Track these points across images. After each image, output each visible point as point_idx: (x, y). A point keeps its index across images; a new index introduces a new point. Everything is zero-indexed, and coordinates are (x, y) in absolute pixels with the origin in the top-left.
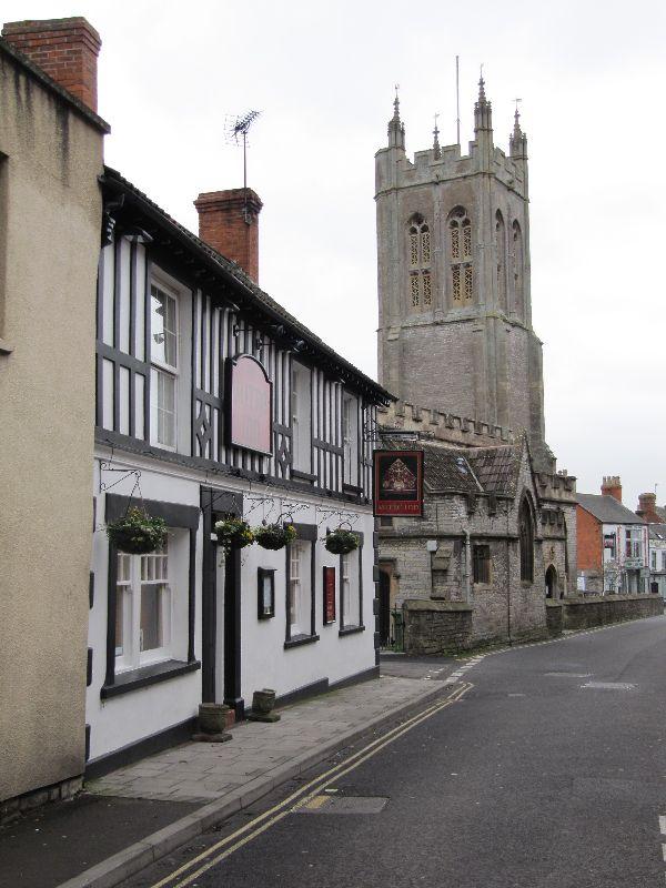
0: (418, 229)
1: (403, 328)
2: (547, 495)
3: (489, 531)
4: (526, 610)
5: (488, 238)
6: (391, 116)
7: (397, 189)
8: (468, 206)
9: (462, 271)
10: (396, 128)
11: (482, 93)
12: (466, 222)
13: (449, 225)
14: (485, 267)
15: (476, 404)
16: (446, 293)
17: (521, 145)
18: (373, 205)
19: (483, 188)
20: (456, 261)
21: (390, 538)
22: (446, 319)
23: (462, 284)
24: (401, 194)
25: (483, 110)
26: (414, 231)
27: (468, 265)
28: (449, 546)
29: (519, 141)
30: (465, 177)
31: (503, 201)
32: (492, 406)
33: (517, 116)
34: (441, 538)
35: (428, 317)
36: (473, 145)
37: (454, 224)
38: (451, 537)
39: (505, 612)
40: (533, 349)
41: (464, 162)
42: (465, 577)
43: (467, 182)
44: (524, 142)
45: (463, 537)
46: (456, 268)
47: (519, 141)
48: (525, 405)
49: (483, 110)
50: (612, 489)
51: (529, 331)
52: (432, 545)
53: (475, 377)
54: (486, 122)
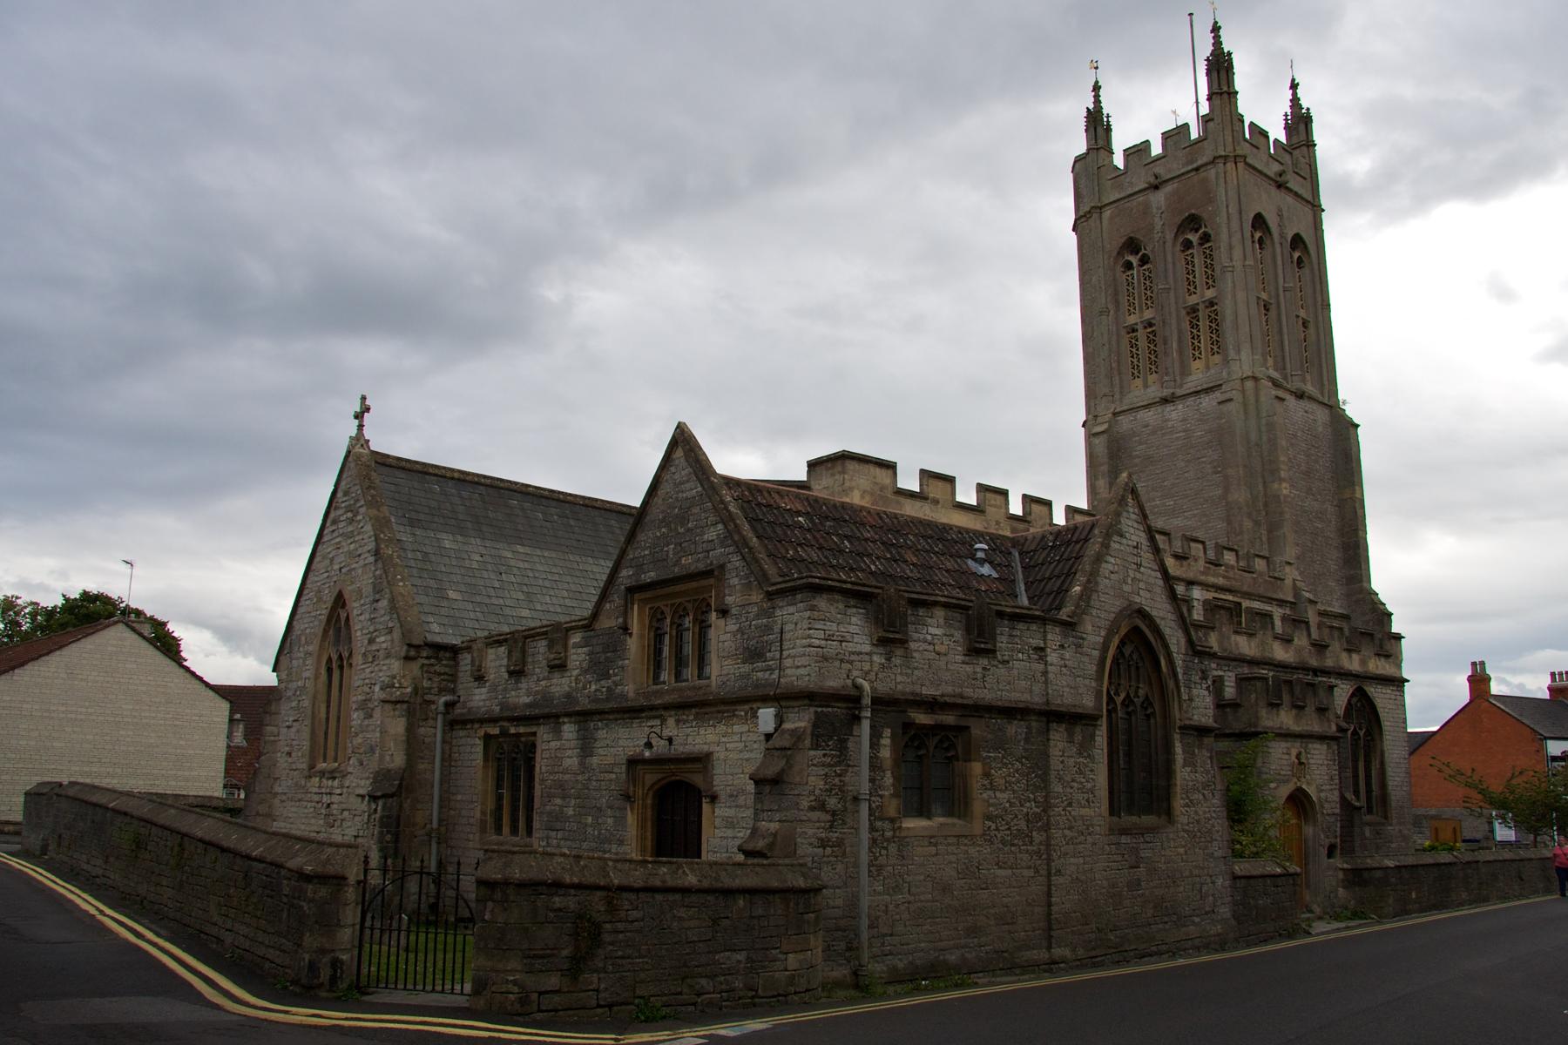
0: (1134, 260)
1: (1114, 414)
2: (1329, 663)
3: (968, 692)
5: (1237, 254)
9: (1202, 313)
10: (1097, 124)
11: (1295, 101)
12: (1206, 238)
13: (1178, 247)
14: (1238, 301)
15: (1229, 523)
16: (1181, 352)
20: (1193, 300)
22: (1179, 392)
24: (1107, 213)
25: (1220, 67)
26: (1129, 266)
27: (1211, 303)
28: (800, 720)
29: (1299, 122)
30: (1197, 169)
31: (1267, 202)
32: (1257, 523)
33: (1294, 86)
34: (784, 699)
35: (1155, 392)
36: (1206, 120)
38: (809, 697)
40: (1344, 431)
42: (856, 799)
43: (1202, 174)
45: (851, 699)
46: (1193, 310)
47: (1299, 122)
52: (766, 716)
54: (1224, 82)
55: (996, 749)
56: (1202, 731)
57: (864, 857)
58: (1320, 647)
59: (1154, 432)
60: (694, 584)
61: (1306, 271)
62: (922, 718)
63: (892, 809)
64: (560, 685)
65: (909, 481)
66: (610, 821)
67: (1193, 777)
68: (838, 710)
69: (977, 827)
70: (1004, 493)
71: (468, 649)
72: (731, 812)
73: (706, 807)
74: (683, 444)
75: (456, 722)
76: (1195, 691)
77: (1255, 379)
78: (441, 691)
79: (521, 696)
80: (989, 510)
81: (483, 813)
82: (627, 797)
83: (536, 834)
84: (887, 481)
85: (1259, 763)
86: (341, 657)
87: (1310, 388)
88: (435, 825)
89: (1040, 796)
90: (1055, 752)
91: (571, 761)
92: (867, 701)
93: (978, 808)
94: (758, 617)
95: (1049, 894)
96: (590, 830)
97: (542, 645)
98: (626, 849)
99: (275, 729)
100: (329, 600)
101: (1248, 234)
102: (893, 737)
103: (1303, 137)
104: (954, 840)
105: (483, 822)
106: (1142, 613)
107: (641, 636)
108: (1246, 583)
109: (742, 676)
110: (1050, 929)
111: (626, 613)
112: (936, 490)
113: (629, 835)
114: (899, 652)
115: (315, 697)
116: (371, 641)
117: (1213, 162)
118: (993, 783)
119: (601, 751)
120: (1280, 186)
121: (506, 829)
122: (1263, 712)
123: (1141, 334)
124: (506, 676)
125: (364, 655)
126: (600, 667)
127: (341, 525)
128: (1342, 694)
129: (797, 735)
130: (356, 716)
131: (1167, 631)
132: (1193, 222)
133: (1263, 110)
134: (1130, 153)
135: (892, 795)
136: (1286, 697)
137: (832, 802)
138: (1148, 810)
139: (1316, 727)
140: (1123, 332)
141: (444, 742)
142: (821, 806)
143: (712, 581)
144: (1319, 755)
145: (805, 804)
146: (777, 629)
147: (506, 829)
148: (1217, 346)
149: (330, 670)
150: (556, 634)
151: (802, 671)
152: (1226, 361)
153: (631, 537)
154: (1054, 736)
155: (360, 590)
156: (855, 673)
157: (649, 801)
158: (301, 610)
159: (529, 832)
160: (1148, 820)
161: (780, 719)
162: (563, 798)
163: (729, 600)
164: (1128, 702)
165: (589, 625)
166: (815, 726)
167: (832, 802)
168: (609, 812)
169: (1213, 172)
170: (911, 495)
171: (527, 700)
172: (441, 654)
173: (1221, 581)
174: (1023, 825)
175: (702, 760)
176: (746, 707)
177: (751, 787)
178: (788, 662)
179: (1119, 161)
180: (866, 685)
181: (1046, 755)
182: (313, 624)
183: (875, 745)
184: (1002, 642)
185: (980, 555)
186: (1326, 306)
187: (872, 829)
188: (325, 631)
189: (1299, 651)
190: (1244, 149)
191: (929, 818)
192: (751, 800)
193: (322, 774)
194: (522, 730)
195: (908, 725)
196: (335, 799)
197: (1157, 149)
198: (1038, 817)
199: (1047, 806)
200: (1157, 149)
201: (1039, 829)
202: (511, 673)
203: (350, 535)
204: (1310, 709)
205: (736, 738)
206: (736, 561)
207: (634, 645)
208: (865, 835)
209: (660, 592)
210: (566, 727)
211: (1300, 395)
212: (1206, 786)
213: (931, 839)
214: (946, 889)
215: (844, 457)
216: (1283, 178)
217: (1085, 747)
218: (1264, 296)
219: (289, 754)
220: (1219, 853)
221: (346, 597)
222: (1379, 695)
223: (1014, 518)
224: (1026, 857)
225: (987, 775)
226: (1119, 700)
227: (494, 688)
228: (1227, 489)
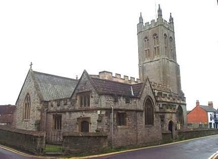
0: (146, 40)
2: (175, 102)
4: (148, 135)
6: (140, 16)
7: (141, 32)
8: (157, 33)
10: (141, 18)
20: (155, 46)
21: (87, 110)
23: (157, 52)
25: (160, 11)
27: (158, 47)
28: (104, 113)
29: (171, 19)
34: (101, 109)
35: (149, 60)
37: (154, 38)
38: (105, 109)
39: (136, 136)
41: (156, 23)
45: (111, 109)
46: (155, 48)
47: (171, 19)
48: (176, 80)
49: (160, 11)
50: (211, 104)
51: (176, 63)
58: (174, 99)
62: (120, 112)
64: (66, 107)
67: (156, 119)
78: (46, 108)
93: (127, 124)
100: (26, 93)
106: (149, 96)
111: (76, 97)
113: (77, 130)
117: (158, 26)
118: (129, 120)
123: (147, 51)
129: (103, 115)
133: (166, 17)
137: (108, 124)
138: (151, 124)
149: (26, 105)
150: (65, 99)
159: (61, 129)
160: (150, 125)
161: (101, 112)
177: (97, 122)
179: (144, 24)
183: (114, 116)
197: (150, 23)
207: (78, 102)
213: (121, 129)
214: (123, 135)
217: (142, 115)
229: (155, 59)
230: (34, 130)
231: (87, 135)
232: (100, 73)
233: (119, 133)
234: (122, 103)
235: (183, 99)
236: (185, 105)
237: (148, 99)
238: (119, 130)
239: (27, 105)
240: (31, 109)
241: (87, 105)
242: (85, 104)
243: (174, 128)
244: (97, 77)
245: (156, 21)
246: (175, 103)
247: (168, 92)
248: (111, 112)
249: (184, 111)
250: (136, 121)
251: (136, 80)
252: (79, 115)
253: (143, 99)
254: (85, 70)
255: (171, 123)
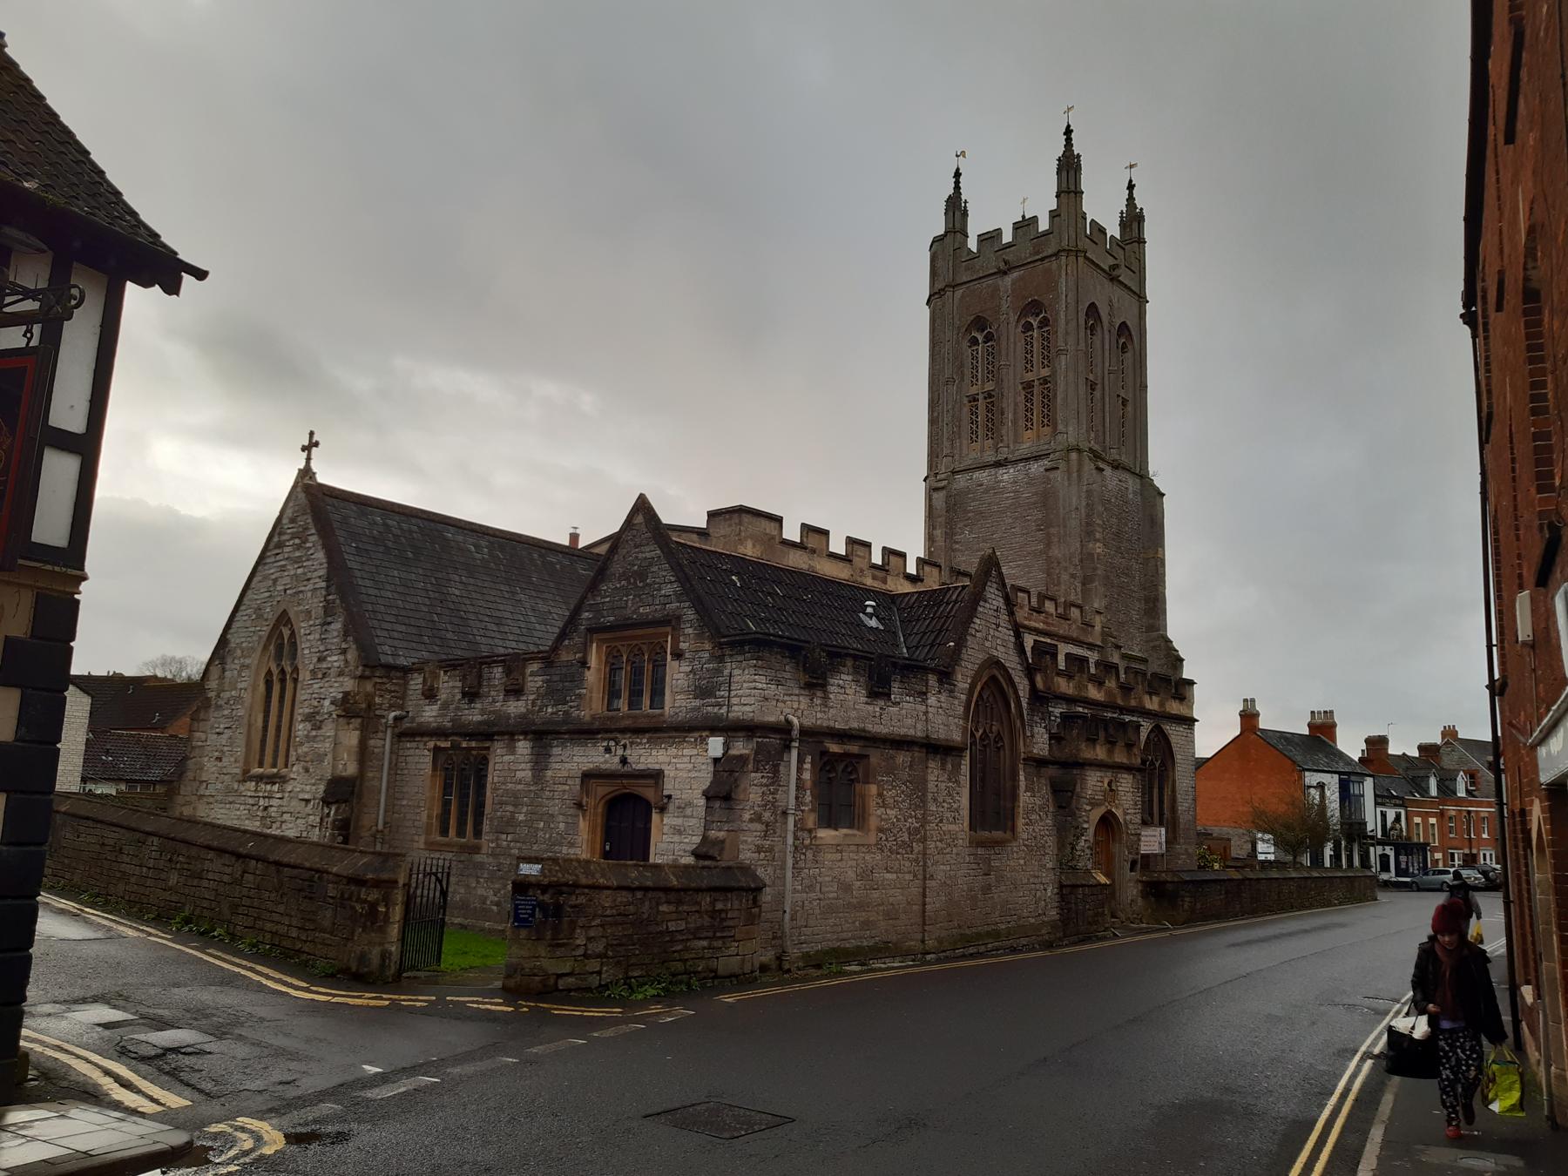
2: (1133, 703)
3: (869, 727)
4: (987, 889)
10: (956, 208)
11: (1131, 199)
13: (1020, 329)
16: (1015, 422)
17: (1135, 225)
18: (926, 312)
19: (1066, 275)
20: (1029, 376)
24: (959, 293)
25: (1069, 166)
26: (974, 342)
27: (1045, 381)
28: (741, 748)
29: (1133, 219)
30: (1042, 259)
31: (1102, 293)
32: (1073, 576)
33: (1131, 187)
34: (731, 729)
36: (1053, 215)
37: (1028, 327)
38: (749, 729)
39: (915, 890)
43: (1046, 264)
44: (1077, 169)
45: (783, 729)
46: (1028, 386)
47: (1133, 219)
49: (1069, 166)
50: (1323, 729)
52: (716, 746)
53: (1048, 534)
54: (1072, 181)
55: (888, 774)
56: (1040, 763)
57: (790, 862)
58: (1126, 689)
59: (986, 491)
60: (651, 631)
61: (1129, 355)
62: (834, 748)
63: (811, 820)
64: (515, 708)
65: (792, 533)
66: (562, 826)
67: (1031, 798)
68: (774, 741)
69: (872, 839)
70: (868, 545)
71: (420, 670)
72: (679, 821)
73: (655, 817)
74: (642, 507)
75: (408, 733)
76: (1036, 730)
77: (1079, 451)
78: (391, 707)
79: (474, 715)
80: (856, 560)
81: (429, 817)
82: (579, 806)
83: (485, 837)
84: (775, 533)
85: (1078, 789)
86: (283, 672)
87: (1124, 459)
88: (380, 827)
89: (919, 813)
90: (931, 778)
91: (525, 773)
92: (795, 733)
93: (873, 822)
94: (709, 662)
95: (924, 896)
96: (540, 833)
97: (498, 672)
98: (578, 851)
99: (203, 736)
100: (270, 614)
101: (1082, 322)
102: (812, 763)
103: (1135, 233)
104: (853, 848)
105: (429, 825)
106: (998, 664)
107: (599, 670)
108: (1063, 628)
109: (698, 709)
110: (924, 924)
111: (585, 650)
112: (813, 541)
113: (581, 841)
114: (819, 694)
115: (251, 708)
116: (320, 660)
117: (1056, 254)
118: (884, 802)
119: (557, 766)
120: (1114, 279)
121: (452, 832)
122: (1083, 746)
123: (981, 403)
124: (459, 696)
125: (313, 672)
126: (555, 693)
127: (287, 549)
128: (1146, 727)
129: (742, 759)
130: (301, 729)
131: (1017, 680)
132: (1035, 307)
133: (1102, 207)
134: (984, 239)
135: (811, 810)
136: (1102, 734)
137: (767, 816)
138: (996, 826)
139: (1120, 757)
140: (965, 400)
141: (391, 752)
142: (757, 818)
143: (669, 629)
144: (1126, 783)
145: (747, 816)
146: (726, 672)
147: (452, 832)
148: (1049, 419)
149: (269, 684)
150: (514, 664)
151: (747, 708)
152: (1055, 432)
153: (593, 587)
154: (932, 764)
155: (309, 612)
156: (787, 710)
157: (600, 810)
158: (235, 625)
159: (478, 833)
160: (998, 834)
161: (727, 746)
162: (515, 806)
163: (683, 646)
164: (985, 735)
165: (548, 660)
166: (756, 753)
167: (767, 816)
168: (561, 818)
169: (1054, 265)
170: (793, 544)
171: (478, 718)
172: (393, 674)
173: (1041, 626)
174: (906, 837)
175: (657, 776)
176: (696, 735)
177: (702, 802)
178: (734, 701)
179: (972, 244)
180: (796, 721)
181: (925, 781)
182: (251, 636)
183: (800, 770)
184: (896, 687)
185: (869, 610)
186: (1143, 387)
187: (796, 838)
188: (265, 648)
189: (1109, 693)
190: (1084, 244)
191: (836, 829)
192: (702, 812)
193: (259, 778)
194: (473, 744)
195: (824, 753)
196: (274, 802)
197: (1007, 237)
198: (917, 830)
199: (924, 822)
200: (1007, 237)
201: (919, 841)
202: (464, 694)
203: (298, 560)
204: (1121, 744)
205: (686, 759)
206: (690, 614)
207: (593, 676)
208: (790, 840)
209: (618, 634)
210: (521, 744)
211: (1116, 466)
212: (1041, 808)
213: (838, 848)
214: (846, 888)
215: (741, 511)
216: (1115, 273)
217: (954, 775)
218: (1091, 377)
219: (219, 759)
220: (1050, 865)
221: (292, 615)
222: (1174, 732)
223: (874, 566)
224: (907, 864)
225: (880, 795)
226: (978, 735)
227: (445, 706)
228: (1048, 545)
229: (1025, 448)
230: (315, 836)
231: (634, 876)
232: (712, 515)
233: (827, 877)
234: (847, 703)
235: (1181, 689)
236: (1190, 722)
237: (993, 678)
238: (829, 857)
239: (280, 682)
240: (301, 711)
241: (646, 700)
242: (634, 702)
243: (1122, 854)
244: (694, 541)
245: (1044, 225)
246: (1131, 711)
247: (1091, 646)
248: (788, 748)
249: (1178, 757)
250: (924, 801)
251: (911, 569)
252: (594, 757)
253: (962, 682)
254: (803, 525)
255: (1108, 823)
